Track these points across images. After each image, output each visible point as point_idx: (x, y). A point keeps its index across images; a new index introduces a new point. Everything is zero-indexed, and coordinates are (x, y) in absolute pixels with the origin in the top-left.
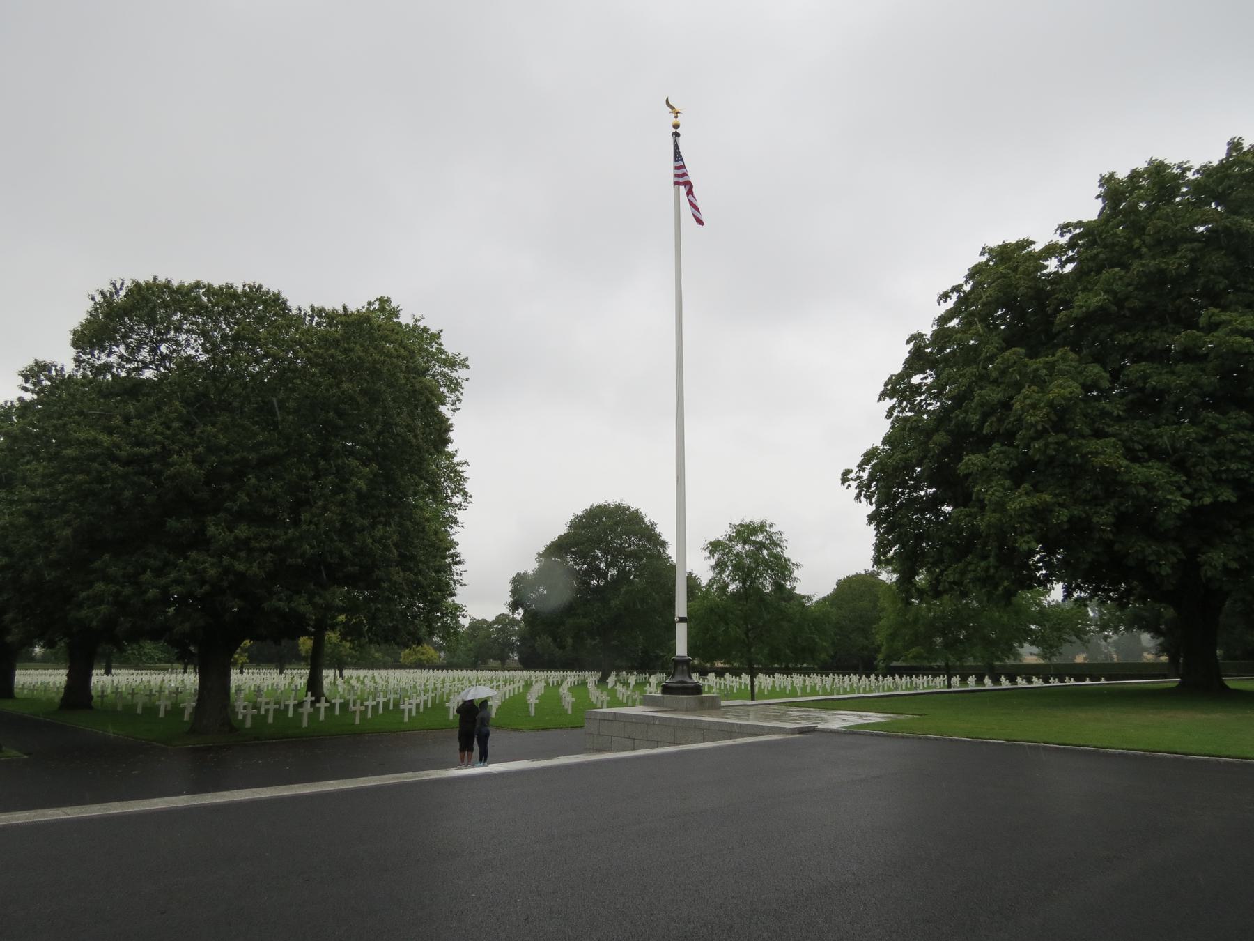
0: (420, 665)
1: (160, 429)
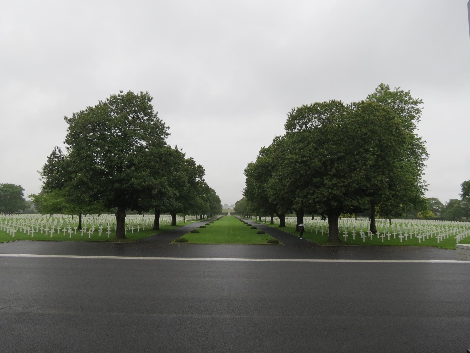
0: (426, 218)
1: (308, 152)
